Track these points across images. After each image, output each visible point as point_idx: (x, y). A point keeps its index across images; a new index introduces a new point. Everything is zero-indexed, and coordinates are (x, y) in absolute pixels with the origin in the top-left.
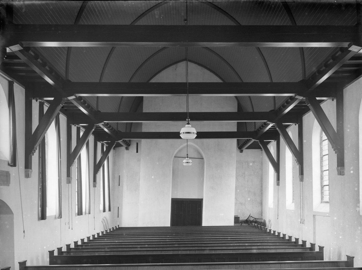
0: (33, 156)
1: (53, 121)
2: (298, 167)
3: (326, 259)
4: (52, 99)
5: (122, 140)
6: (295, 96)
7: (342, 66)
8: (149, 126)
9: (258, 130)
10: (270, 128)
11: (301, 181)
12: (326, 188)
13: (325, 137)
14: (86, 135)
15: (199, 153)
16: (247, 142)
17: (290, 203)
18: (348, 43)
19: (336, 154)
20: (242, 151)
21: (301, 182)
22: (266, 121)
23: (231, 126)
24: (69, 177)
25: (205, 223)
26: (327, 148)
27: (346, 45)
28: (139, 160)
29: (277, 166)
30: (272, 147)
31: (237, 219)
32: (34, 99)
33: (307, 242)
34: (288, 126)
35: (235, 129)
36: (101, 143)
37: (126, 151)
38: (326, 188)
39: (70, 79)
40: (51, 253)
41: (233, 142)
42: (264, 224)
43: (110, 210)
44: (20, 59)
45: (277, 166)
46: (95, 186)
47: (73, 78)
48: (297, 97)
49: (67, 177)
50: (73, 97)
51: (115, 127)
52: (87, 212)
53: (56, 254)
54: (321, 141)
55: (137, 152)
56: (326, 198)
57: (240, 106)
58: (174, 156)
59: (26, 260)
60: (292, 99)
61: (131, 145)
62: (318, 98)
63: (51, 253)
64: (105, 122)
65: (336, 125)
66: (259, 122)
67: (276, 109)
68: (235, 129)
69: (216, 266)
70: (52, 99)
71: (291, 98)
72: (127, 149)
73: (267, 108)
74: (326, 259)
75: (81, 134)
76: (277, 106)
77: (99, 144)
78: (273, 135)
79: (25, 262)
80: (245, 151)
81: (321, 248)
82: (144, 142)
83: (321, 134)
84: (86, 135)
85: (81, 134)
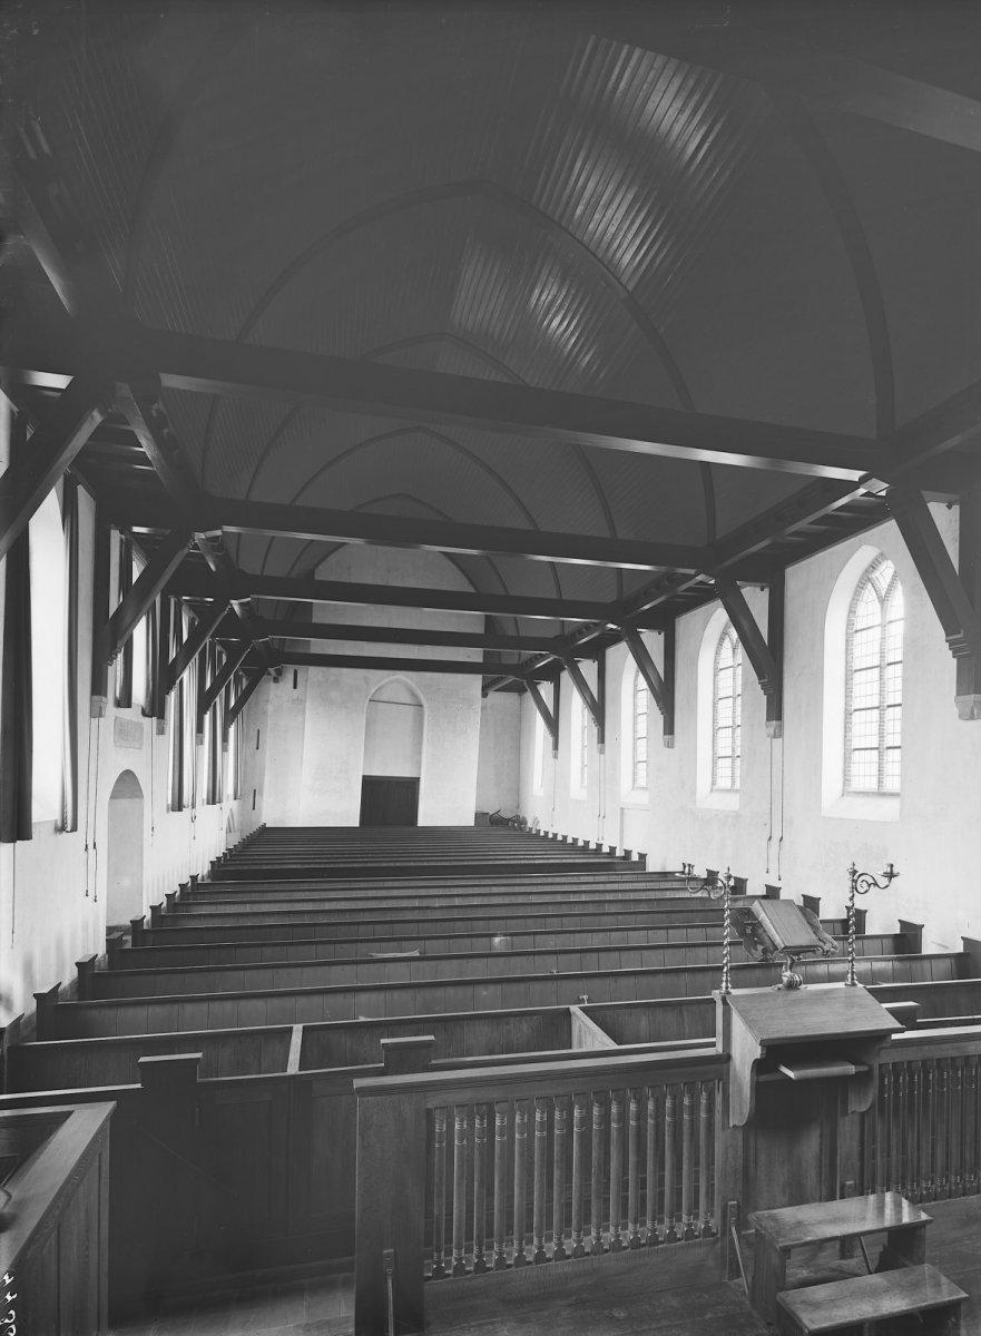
1: (53, 491)
2: (595, 730)
3: (650, 869)
8: (320, 646)
9: (526, 662)
12: (642, 766)
15: (413, 695)
17: (577, 788)
18: (862, 473)
19: (955, 660)
21: (778, 741)
23: (474, 655)
24: (163, 718)
25: (421, 823)
26: (645, 703)
28: (301, 701)
29: (553, 724)
31: (478, 816)
35: (480, 629)
38: (642, 766)
41: (475, 682)
42: (523, 822)
45: (553, 724)
52: (203, 793)
54: (636, 691)
55: (295, 687)
56: (642, 782)
58: (369, 697)
65: (663, 667)
68: (480, 629)
69: (444, 962)
71: (586, 626)
72: (276, 680)
73: (551, 633)
74: (650, 869)
78: (552, 673)
81: (642, 857)
82: (314, 673)
83: (637, 676)
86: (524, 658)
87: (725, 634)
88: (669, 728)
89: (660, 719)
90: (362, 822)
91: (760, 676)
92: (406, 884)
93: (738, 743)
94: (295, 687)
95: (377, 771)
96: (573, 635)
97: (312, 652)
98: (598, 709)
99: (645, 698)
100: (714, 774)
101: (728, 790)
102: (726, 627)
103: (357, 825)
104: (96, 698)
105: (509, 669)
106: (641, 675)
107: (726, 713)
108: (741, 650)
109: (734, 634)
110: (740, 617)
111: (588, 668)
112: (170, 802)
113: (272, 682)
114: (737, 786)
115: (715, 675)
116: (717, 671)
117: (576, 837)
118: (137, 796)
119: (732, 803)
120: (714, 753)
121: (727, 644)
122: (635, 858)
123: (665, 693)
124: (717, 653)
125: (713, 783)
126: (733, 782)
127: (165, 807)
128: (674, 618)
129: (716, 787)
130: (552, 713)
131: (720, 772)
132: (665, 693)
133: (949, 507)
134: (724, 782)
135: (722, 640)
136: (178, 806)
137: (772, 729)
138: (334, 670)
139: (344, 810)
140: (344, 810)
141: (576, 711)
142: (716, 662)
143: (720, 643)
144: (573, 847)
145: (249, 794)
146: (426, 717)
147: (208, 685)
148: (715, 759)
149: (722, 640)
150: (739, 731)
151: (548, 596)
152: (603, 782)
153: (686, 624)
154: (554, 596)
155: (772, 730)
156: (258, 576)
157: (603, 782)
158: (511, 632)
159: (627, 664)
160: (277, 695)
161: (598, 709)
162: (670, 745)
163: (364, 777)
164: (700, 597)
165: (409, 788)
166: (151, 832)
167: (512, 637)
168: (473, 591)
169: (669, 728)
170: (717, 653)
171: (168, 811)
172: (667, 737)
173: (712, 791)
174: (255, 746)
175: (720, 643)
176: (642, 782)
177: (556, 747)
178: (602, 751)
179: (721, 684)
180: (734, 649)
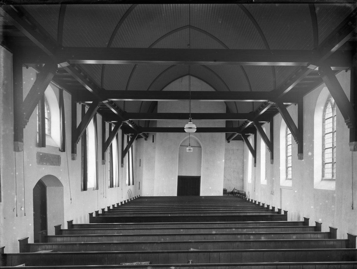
0: (24, 129)
3: (289, 220)
4: (91, 102)
5: (128, 121)
7: (310, 74)
8: (162, 123)
10: (249, 125)
11: (272, 164)
12: (290, 169)
14: (116, 129)
15: (198, 143)
16: (233, 134)
19: (349, 129)
20: (229, 142)
23: (221, 123)
25: (202, 194)
28: (154, 148)
31: (225, 191)
32: (78, 102)
33: (337, 230)
34: (263, 123)
36: (109, 123)
37: (145, 141)
38: (290, 169)
40: (91, 215)
43: (133, 184)
44: (67, 72)
45: (254, 153)
46: (122, 166)
47: (107, 87)
49: (102, 159)
50: (107, 101)
54: (287, 135)
55: (153, 142)
56: (290, 176)
57: (228, 109)
60: (266, 104)
62: (284, 104)
70: (91, 102)
71: (265, 103)
72: (146, 139)
74: (289, 220)
75: (113, 128)
76: (255, 109)
77: (79, 107)
78: (252, 130)
79: (72, 221)
81: (286, 212)
83: (287, 129)
84: (116, 129)
85: (113, 128)
87: (328, 101)
93: (335, 155)
94: (153, 142)
95: (185, 174)
98: (271, 145)
103: (176, 195)
104: (16, 142)
105: (238, 130)
106: (288, 129)
108: (336, 108)
111: (266, 128)
112: (109, 185)
113: (145, 141)
116: (324, 120)
118: (61, 186)
119: (332, 186)
121: (329, 106)
122: (283, 213)
124: (324, 111)
126: (333, 176)
127: (80, 189)
128: (303, 97)
129: (324, 178)
131: (326, 171)
134: (328, 176)
136: (112, 186)
137: (353, 146)
138: (166, 133)
139: (172, 190)
140: (172, 190)
142: (324, 116)
143: (326, 107)
145: (135, 182)
146: (202, 151)
147: (130, 140)
151: (248, 91)
155: (352, 147)
158: (235, 112)
159: (282, 121)
160: (146, 145)
161: (271, 145)
163: (178, 176)
165: (196, 181)
168: (213, 90)
170: (324, 111)
173: (322, 180)
175: (326, 107)
176: (290, 176)
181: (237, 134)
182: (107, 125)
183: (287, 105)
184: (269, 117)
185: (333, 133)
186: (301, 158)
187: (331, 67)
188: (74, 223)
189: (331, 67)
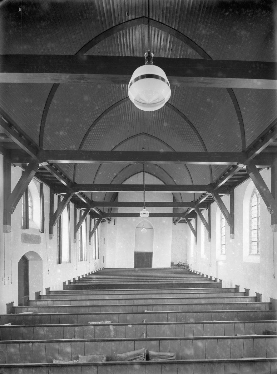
0: (12, 215)
3: (224, 287)
6: (238, 164)
9: (185, 212)
13: (223, 217)
14: (85, 214)
17: (203, 255)
18: (237, 162)
22: (189, 207)
25: (154, 266)
27: (235, 163)
30: (193, 222)
31: (172, 264)
33: (262, 295)
34: (203, 210)
35: (171, 200)
39: (76, 182)
40: (64, 283)
42: (188, 267)
46: (90, 244)
47: (78, 182)
48: (207, 193)
51: (102, 210)
52: (86, 259)
53: (67, 283)
54: (221, 219)
59: (13, 301)
61: (111, 221)
62: (219, 194)
63: (64, 283)
64: (51, 161)
66: (186, 208)
67: (195, 200)
68: (171, 200)
71: (204, 194)
73: (190, 200)
74: (224, 287)
75: (82, 214)
77: (93, 220)
78: (193, 215)
79: (49, 289)
80: (177, 224)
81: (221, 281)
82: (119, 219)
83: (221, 215)
85: (82, 214)
86: (185, 210)
87: (254, 192)
88: (232, 231)
89: (229, 228)
90: (136, 266)
91: (268, 206)
92: (129, 292)
93: (260, 235)
94: (115, 225)
96: (197, 200)
97: (118, 213)
98: (209, 227)
99: (224, 220)
100: (250, 248)
101: (256, 255)
102: (254, 189)
106: (223, 214)
107: (255, 222)
108: (260, 197)
109: (258, 192)
110: (260, 183)
114: (259, 253)
115: (250, 209)
116: (251, 207)
117: (200, 272)
120: (250, 240)
121: (255, 196)
122: (218, 281)
123: (231, 218)
124: (251, 200)
125: (250, 252)
126: (258, 251)
130: (195, 230)
132: (231, 218)
133: (268, 169)
135: (253, 195)
140: (130, 263)
141: (202, 228)
144: (202, 277)
148: (251, 242)
149: (253, 195)
150: (260, 205)
152: (210, 252)
153: (238, 190)
154: (191, 184)
155: (273, 229)
156: (91, 185)
157: (210, 252)
161: (209, 227)
162: (232, 238)
163: (135, 252)
164: (244, 177)
166: (48, 272)
167: (179, 202)
169: (232, 231)
170: (251, 200)
171: (57, 264)
172: (232, 234)
174: (103, 243)
177: (196, 241)
178: (210, 241)
179: (253, 212)
180: (257, 198)
181: (192, 209)
182: (78, 211)
183: (202, 210)
184: (207, 204)
185: (258, 217)
186: (210, 241)
187: (256, 166)
188: (51, 290)
189: (256, 166)
